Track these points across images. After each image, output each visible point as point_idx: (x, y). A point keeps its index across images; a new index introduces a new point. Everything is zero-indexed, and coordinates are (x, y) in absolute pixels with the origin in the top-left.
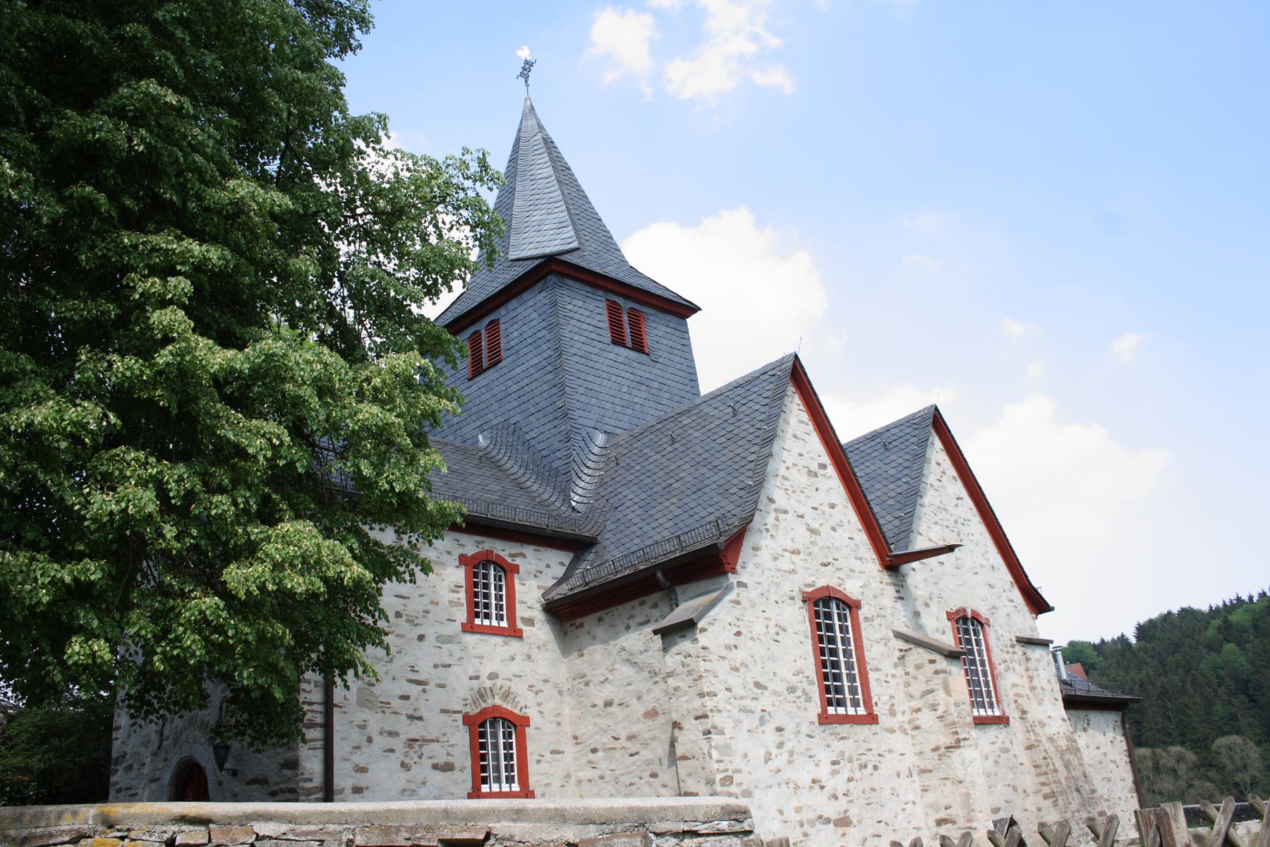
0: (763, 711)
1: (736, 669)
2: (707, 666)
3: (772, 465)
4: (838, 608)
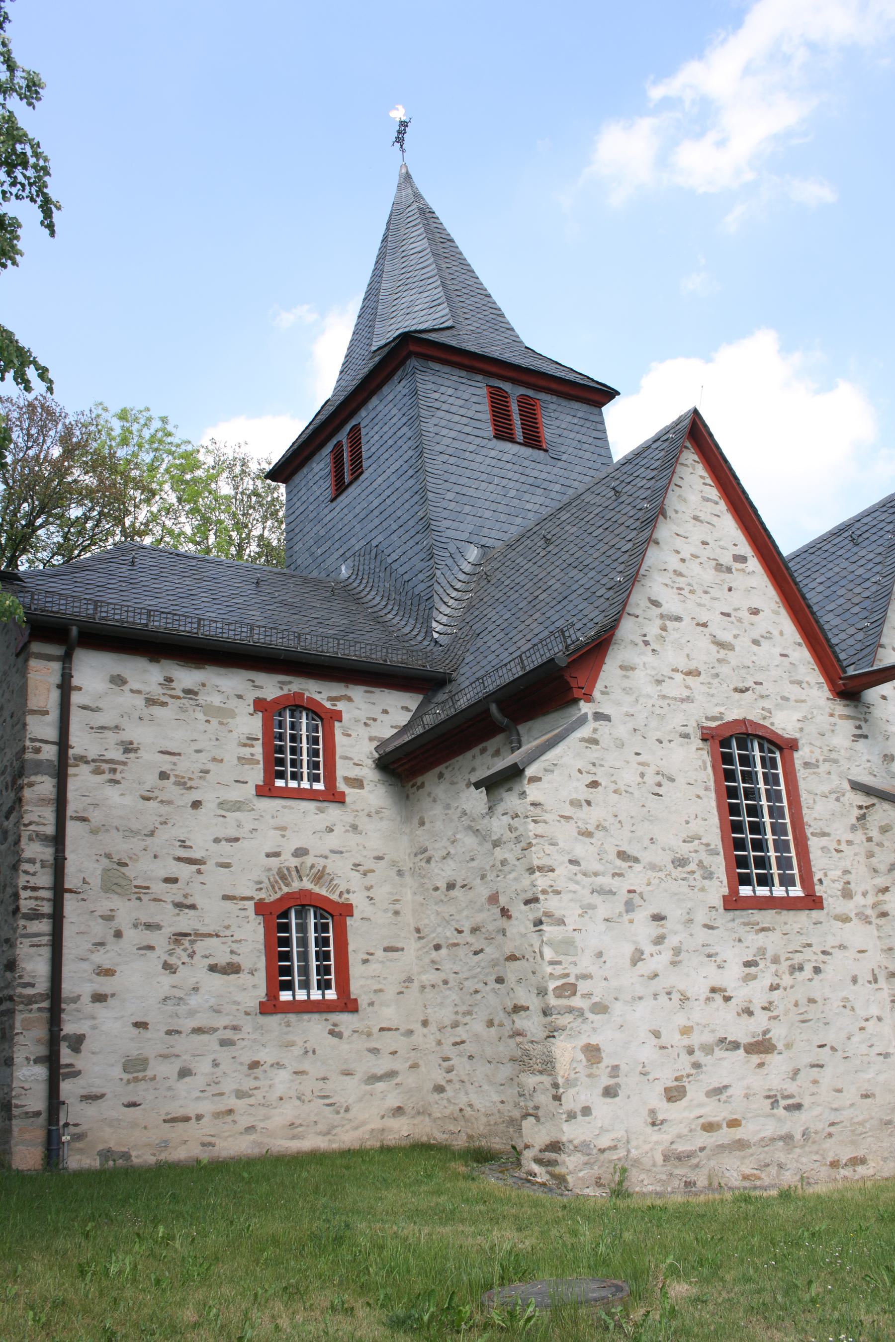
0: (630, 892)
1: (589, 834)
2: (540, 829)
3: (653, 556)
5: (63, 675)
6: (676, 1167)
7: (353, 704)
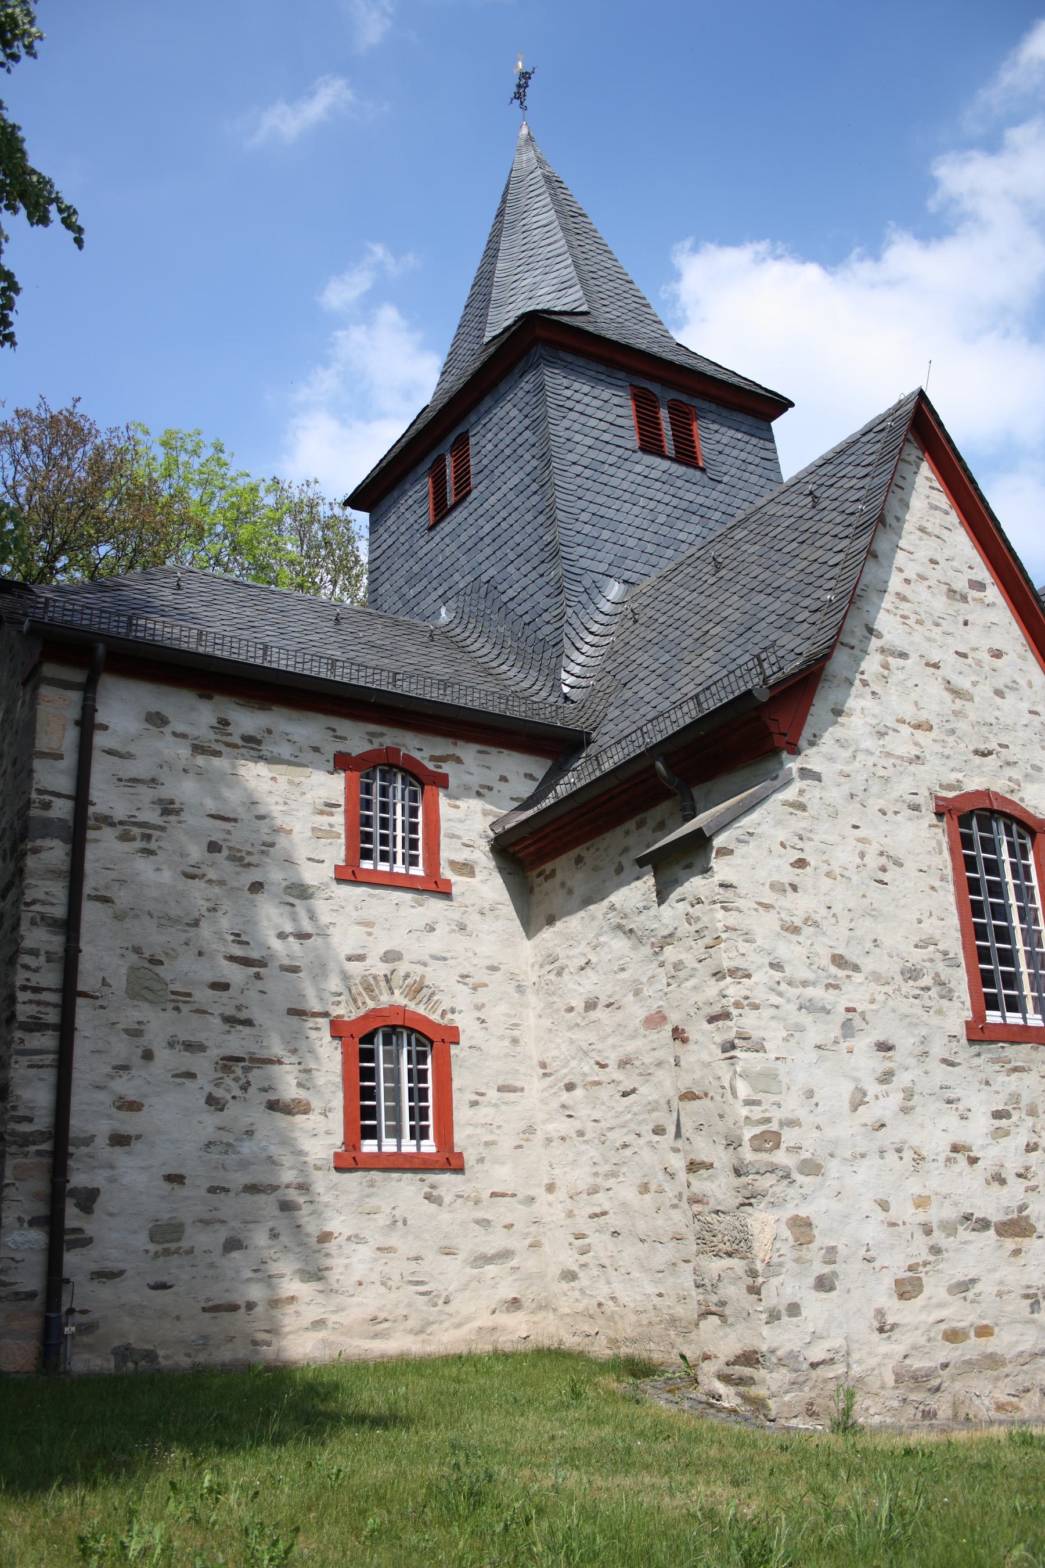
2: (732, 919)
4: (1009, 833)
5: (84, 708)
6: (912, 1390)
7: (463, 767)
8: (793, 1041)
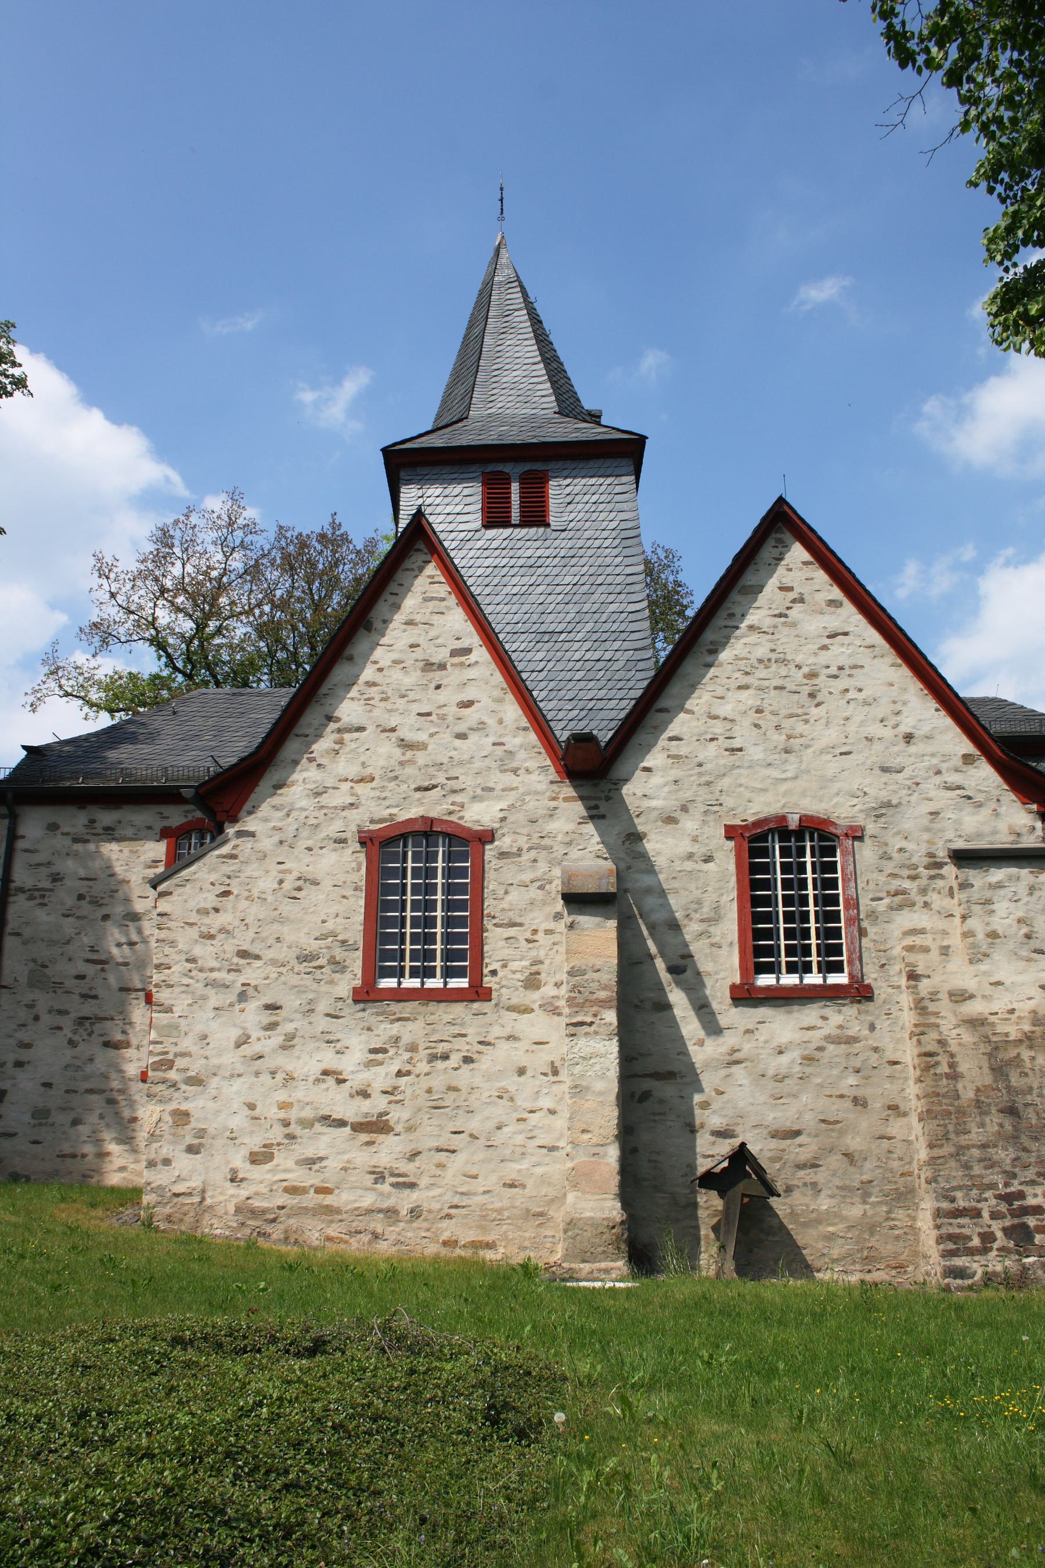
0: (243, 985)
6: (249, 1218)
8: (196, 1006)
